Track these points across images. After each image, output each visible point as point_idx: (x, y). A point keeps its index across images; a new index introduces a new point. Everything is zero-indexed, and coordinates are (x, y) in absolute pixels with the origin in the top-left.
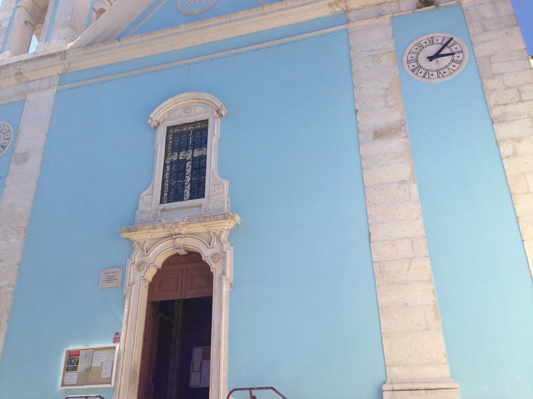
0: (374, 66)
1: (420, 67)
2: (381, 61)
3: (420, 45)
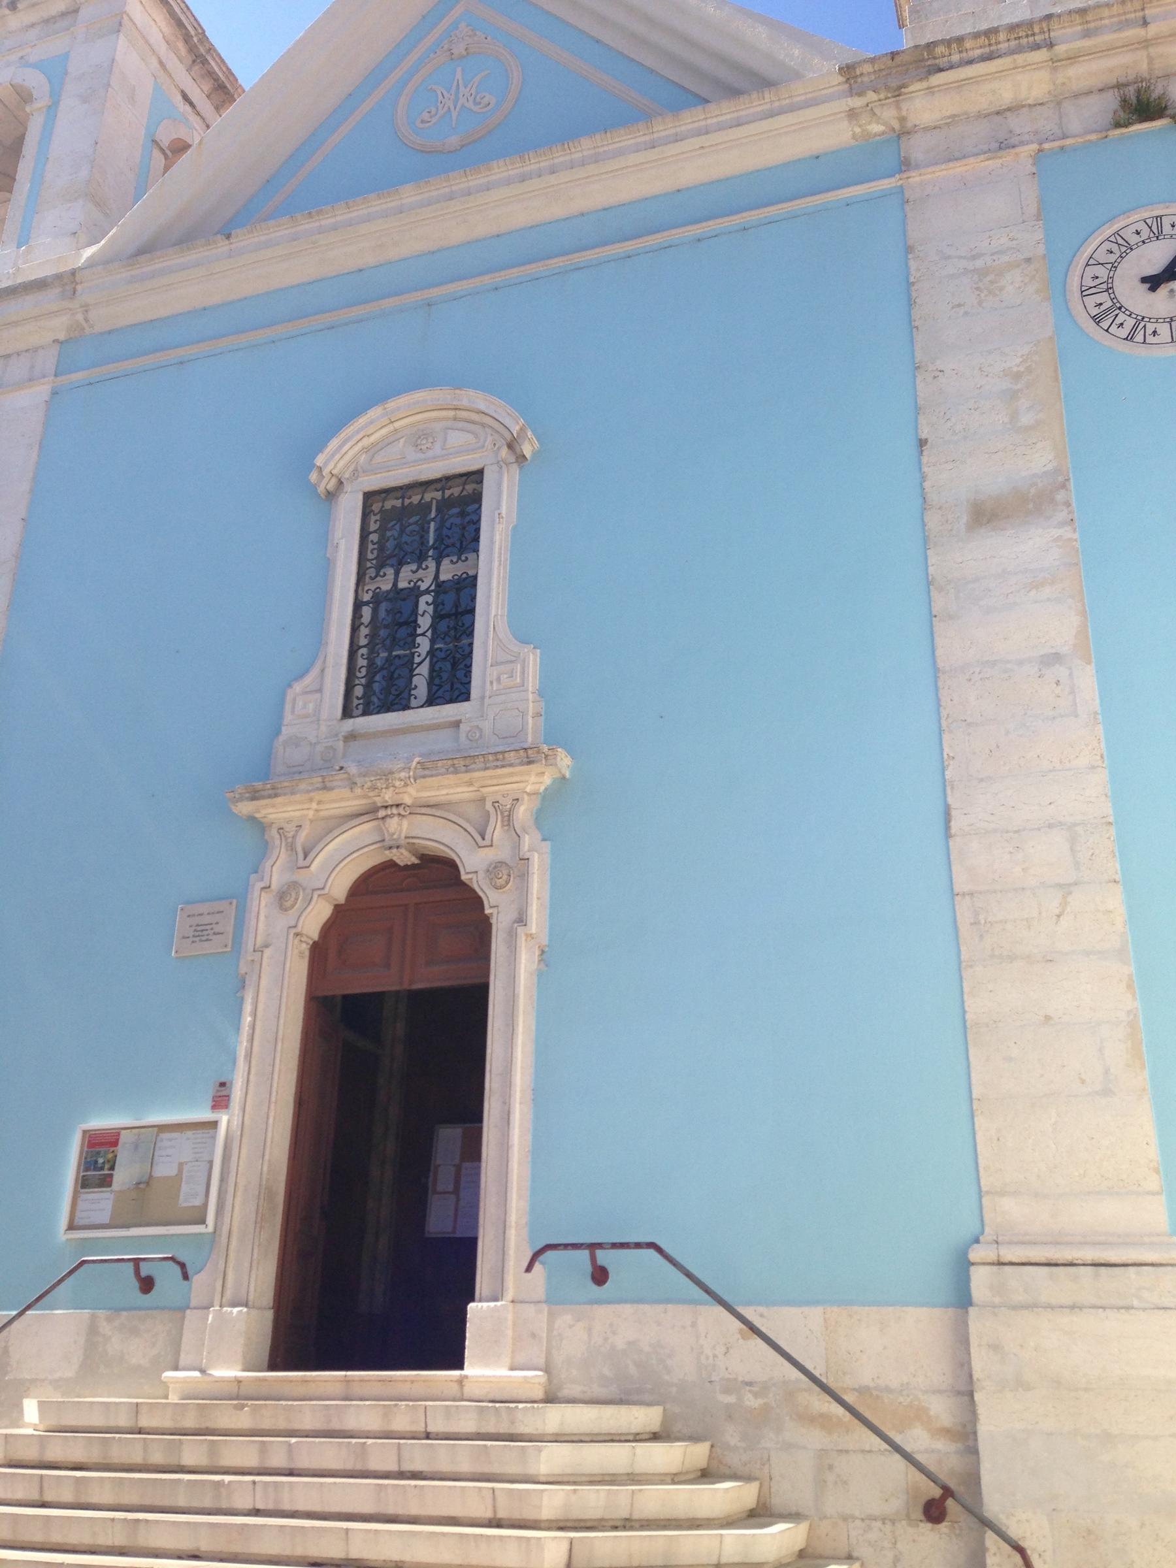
0: (980, 303)
1: (1120, 308)
2: (1001, 289)
3: (1121, 241)
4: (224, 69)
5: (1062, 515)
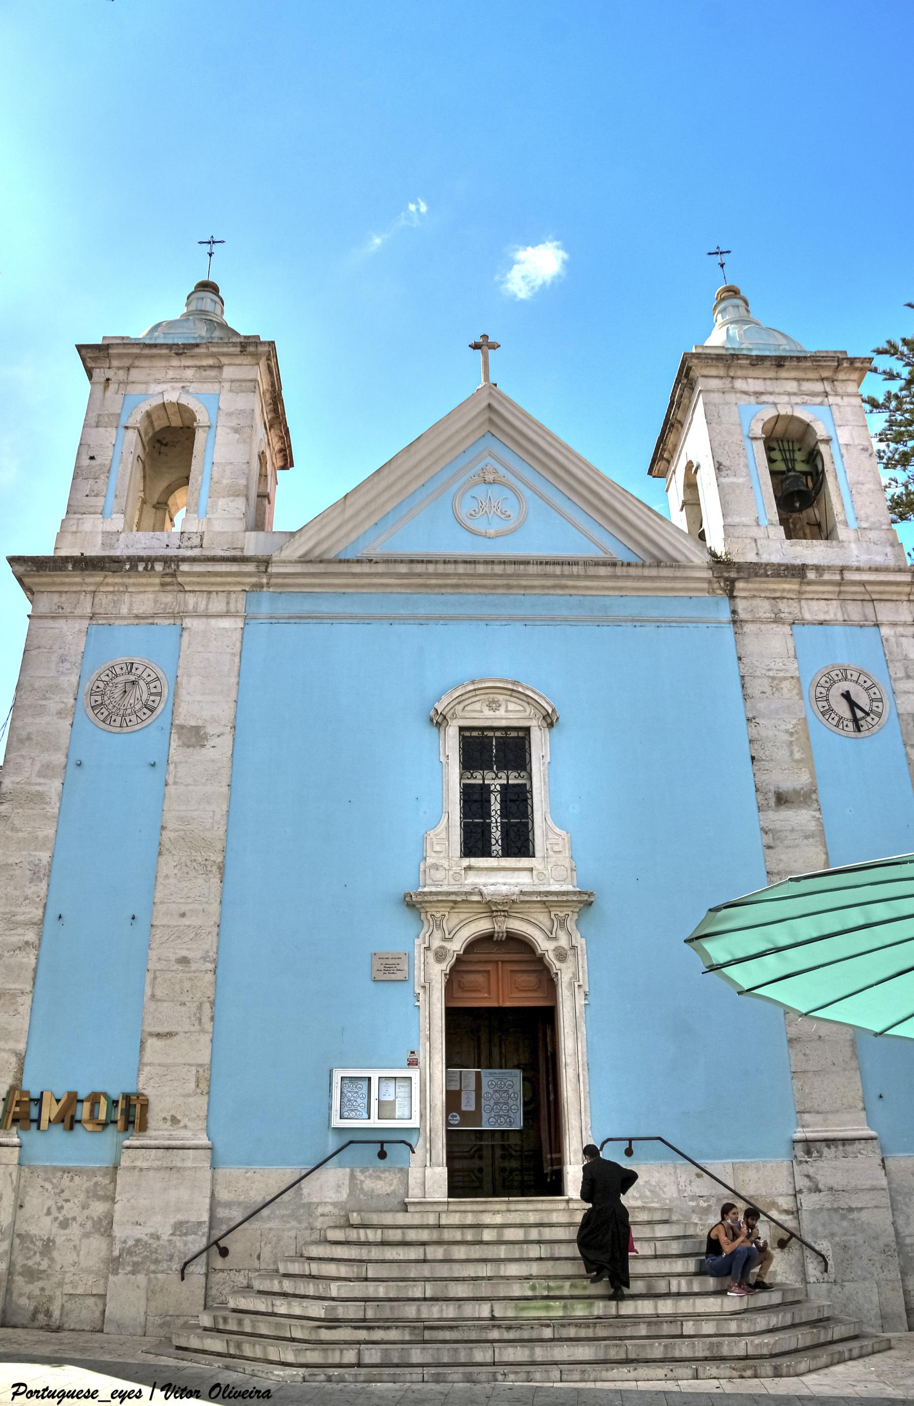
2: (782, 689)
4: (552, 1098)
5: (815, 806)
